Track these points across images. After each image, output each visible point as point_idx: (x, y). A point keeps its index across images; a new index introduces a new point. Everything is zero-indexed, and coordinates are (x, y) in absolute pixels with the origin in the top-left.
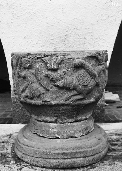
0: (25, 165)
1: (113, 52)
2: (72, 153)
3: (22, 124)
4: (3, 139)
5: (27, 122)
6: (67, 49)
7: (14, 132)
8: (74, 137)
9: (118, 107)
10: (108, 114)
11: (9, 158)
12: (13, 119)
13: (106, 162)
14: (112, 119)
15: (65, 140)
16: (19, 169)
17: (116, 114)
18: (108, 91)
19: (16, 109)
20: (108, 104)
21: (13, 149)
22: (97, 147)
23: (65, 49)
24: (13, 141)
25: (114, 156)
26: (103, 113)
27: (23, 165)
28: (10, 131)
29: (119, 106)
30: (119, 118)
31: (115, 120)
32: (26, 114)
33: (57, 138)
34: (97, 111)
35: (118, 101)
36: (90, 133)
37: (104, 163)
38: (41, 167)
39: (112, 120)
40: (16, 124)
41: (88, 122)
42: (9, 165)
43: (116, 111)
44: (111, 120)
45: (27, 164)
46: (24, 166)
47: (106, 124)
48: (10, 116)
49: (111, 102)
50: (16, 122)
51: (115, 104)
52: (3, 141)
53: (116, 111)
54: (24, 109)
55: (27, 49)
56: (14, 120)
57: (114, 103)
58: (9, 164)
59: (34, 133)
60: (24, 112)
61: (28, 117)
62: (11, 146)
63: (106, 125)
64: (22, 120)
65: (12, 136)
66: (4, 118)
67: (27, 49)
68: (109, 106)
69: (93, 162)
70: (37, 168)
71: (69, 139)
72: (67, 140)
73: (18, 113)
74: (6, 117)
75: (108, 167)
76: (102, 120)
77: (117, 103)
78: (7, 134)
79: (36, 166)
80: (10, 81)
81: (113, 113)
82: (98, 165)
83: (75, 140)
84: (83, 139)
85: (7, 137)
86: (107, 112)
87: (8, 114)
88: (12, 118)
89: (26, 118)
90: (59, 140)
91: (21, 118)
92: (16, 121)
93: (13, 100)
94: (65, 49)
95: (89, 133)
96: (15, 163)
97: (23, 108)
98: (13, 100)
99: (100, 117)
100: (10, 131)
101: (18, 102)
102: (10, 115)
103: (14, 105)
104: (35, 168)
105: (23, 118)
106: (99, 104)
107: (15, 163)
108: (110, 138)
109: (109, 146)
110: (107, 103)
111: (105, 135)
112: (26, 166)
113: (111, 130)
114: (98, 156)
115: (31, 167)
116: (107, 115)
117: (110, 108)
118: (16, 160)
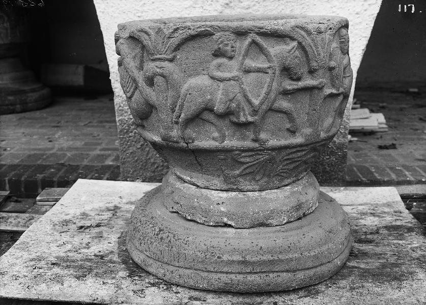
0: (152, 281)
1: (379, 14)
2: (263, 263)
3: (143, 181)
4: (97, 217)
5: (155, 179)
6: (258, 5)
7: (124, 201)
8: (268, 225)
9: (381, 147)
10: (354, 163)
11: (114, 262)
12: (121, 170)
13: (343, 283)
14: (364, 177)
15: (248, 230)
16: (139, 291)
17: (375, 165)
18: (358, 106)
19: (128, 147)
20: (356, 139)
21: (122, 241)
22: (324, 248)
23: (254, 5)
24: (122, 223)
25: (363, 269)
26: (344, 163)
27: (147, 280)
28: (114, 198)
29: (383, 145)
30: (380, 175)
31: (371, 181)
32: (152, 160)
33: (226, 225)
34: (327, 159)
35: (382, 130)
36: (308, 216)
37: (338, 285)
38: (190, 288)
39: (364, 179)
40: (127, 181)
41: (303, 193)
42: (114, 281)
43: (375, 157)
44: (362, 180)
45: (157, 280)
46: (149, 283)
47: (347, 188)
48: (113, 161)
49: (363, 134)
50: (129, 177)
51: (374, 138)
52: (98, 222)
53: (375, 157)
54: (147, 149)
55: (153, 3)
56: (123, 172)
57: (372, 136)
58: (114, 278)
59: (171, 210)
60: (148, 154)
61: (157, 167)
62: (119, 235)
63: (348, 192)
64: (143, 173)
65: (118, 211)
66: (97, 166)
67: (153, 3)
68: (359, 143)
69: (312, 282)
70: (179, 289)
71: (255, 230)
72: (251, 230)
73: (133, 158)
74: (104, 162)
75: (348, 294)
76: (339, 179)
77: (379, 135)
78: (108, 205)
79: (178, 286)
80: (112, 81)
81: (367, 162)
82: (322, 288)
83: (271, 232)
84: (291, 230)
85: (108, 213)
86: (353, 160)
87: (110, 155)
88: (118, 167)
89: (153, 168)
90: (230, 230)
91: (141, 168)
92: (129, 175)
93: (120, 127)
94: (254, 5)
95: (305, 215)
96: (128, 276)
97: (145, 146)
98: (120, 127)
99: (333, 173)
100: (114, 198)
101: (132, 132)
102: (114, 157)
103: (123, 138)
104: (174, 288)
105: (144, 168)
106: (335, 142)
107: (128, 276)
108: (356, 226)
109: (353, 244)
110: (353, 136)
111: (346, 220)
112: (153, 285)
113: (362, 205)
114: (325, 269)
115: (165, 288)
116: (351, 165)
117: (361, 149)
118: (129, 270)
